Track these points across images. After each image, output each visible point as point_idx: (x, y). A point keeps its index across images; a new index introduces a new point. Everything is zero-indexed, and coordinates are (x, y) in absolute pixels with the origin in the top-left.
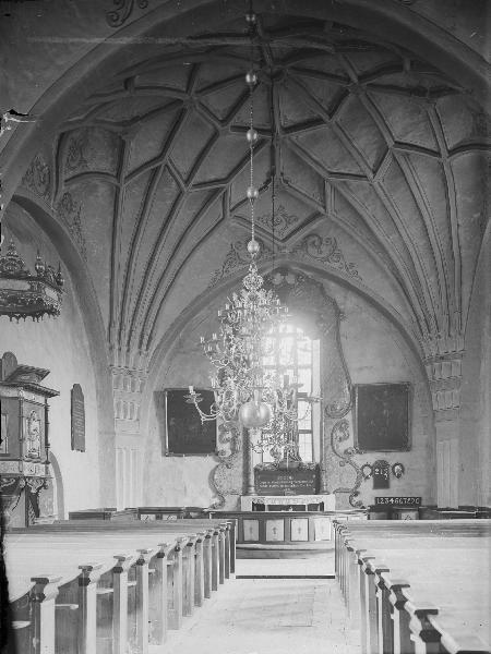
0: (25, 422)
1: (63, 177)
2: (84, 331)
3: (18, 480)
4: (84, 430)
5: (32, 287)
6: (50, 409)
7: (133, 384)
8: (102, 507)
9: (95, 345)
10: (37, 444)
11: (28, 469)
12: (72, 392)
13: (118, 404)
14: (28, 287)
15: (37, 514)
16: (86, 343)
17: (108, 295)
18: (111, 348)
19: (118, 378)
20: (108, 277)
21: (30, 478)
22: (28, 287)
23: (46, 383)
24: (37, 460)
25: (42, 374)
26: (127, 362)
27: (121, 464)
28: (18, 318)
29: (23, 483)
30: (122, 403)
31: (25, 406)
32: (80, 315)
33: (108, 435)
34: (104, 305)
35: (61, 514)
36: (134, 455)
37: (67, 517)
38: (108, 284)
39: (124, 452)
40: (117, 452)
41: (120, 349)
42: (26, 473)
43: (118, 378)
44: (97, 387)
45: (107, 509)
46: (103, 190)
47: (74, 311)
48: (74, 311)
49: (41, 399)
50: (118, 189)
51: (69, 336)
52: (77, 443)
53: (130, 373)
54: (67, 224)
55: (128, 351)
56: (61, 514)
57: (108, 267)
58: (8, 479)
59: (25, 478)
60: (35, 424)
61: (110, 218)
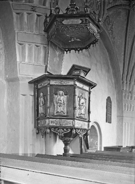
0: (77, 99)
1: (106, 8)
2: (113, 77)
3: (72, 129)
4: (111, 115)
5: (83, 21)
6: (91, 93)
7: (131, 97)
8: (117, 145)
9: (116, 75)
10: (83, 111)
11: (78, 124)
12: (107, 99)
13: (125, 105)
14: (80, 22)
15: (88, 148)
16: (113, 81)
17: (123, 61)
18: (123, 83)
19: (125, 95)
20: (123, 53)
21: (78, 129)
22: (80, 22)
23: (89, 77)
24: (83, 120)
25: (87, 71)
26: (129, 88)
27: (125, 129)
28: (79, 51)
29: (74, 131)
30: (127, 104)
31: (77, 91)
32: (111, 70)
33: (121, 117)
34: (121, 65)
35: (101, 148)
36: (131, 125)
37: (103, 150)
38: (123, 56)
39: (127, 124)
40: (124, 123)
41: (126, 83)
42: (76, 126)
43: (125, 95)
44: (117, 99)
45: (119, 146)
46: (123, 13)
47: (109, 68)
48: (109, 68)
49: (87, 88)
50: (129, 11)
51: (107, 78)
52: (108, 120)
53: (130, 92)
54: (107, 30)
55: (130, 83)
56: (101, 148)
57: (123, 49)
58: (67, 129)
59: (75, 129)
60: (82, 101)
61: (125, 27)
